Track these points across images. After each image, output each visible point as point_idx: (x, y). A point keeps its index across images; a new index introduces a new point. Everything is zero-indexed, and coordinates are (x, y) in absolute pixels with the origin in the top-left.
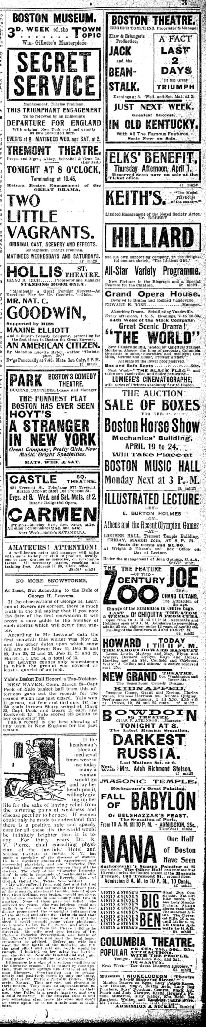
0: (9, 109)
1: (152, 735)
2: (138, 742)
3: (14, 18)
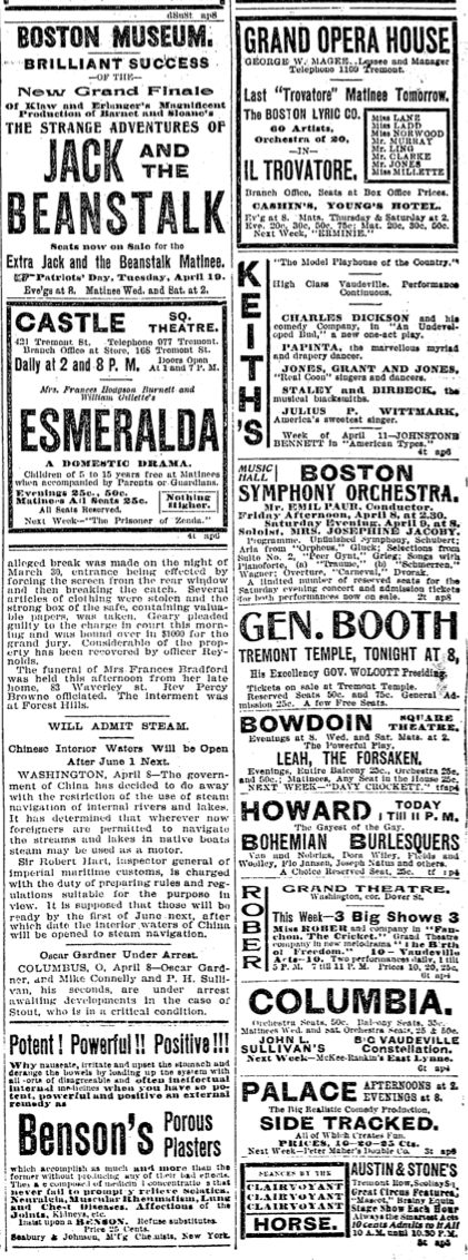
0: (10, 125)
1: (396, 1118)
3: (21, 37)
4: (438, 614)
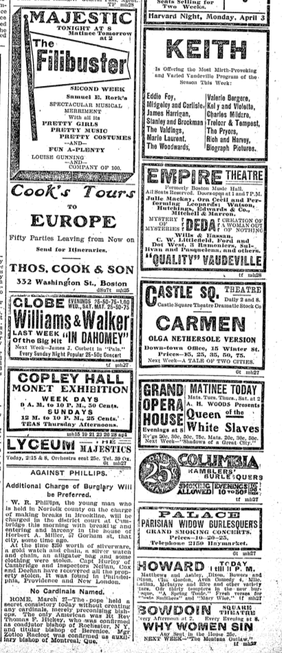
2: (191, 326)
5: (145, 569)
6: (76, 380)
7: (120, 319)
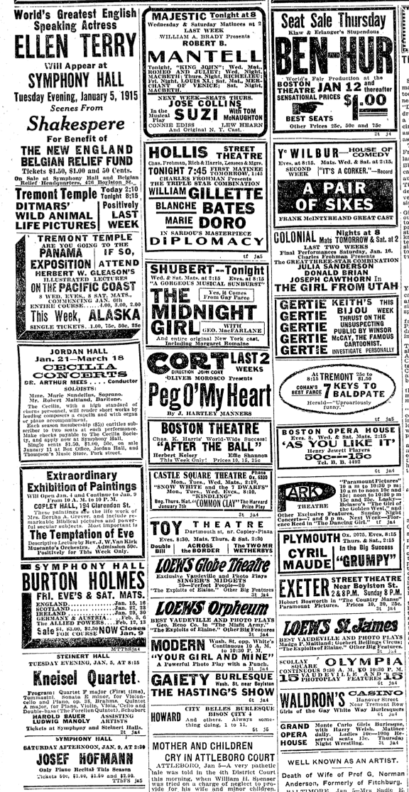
4: (167, 290)
5: (157, 157)
6: (207, 681)
7: (244, 393)
